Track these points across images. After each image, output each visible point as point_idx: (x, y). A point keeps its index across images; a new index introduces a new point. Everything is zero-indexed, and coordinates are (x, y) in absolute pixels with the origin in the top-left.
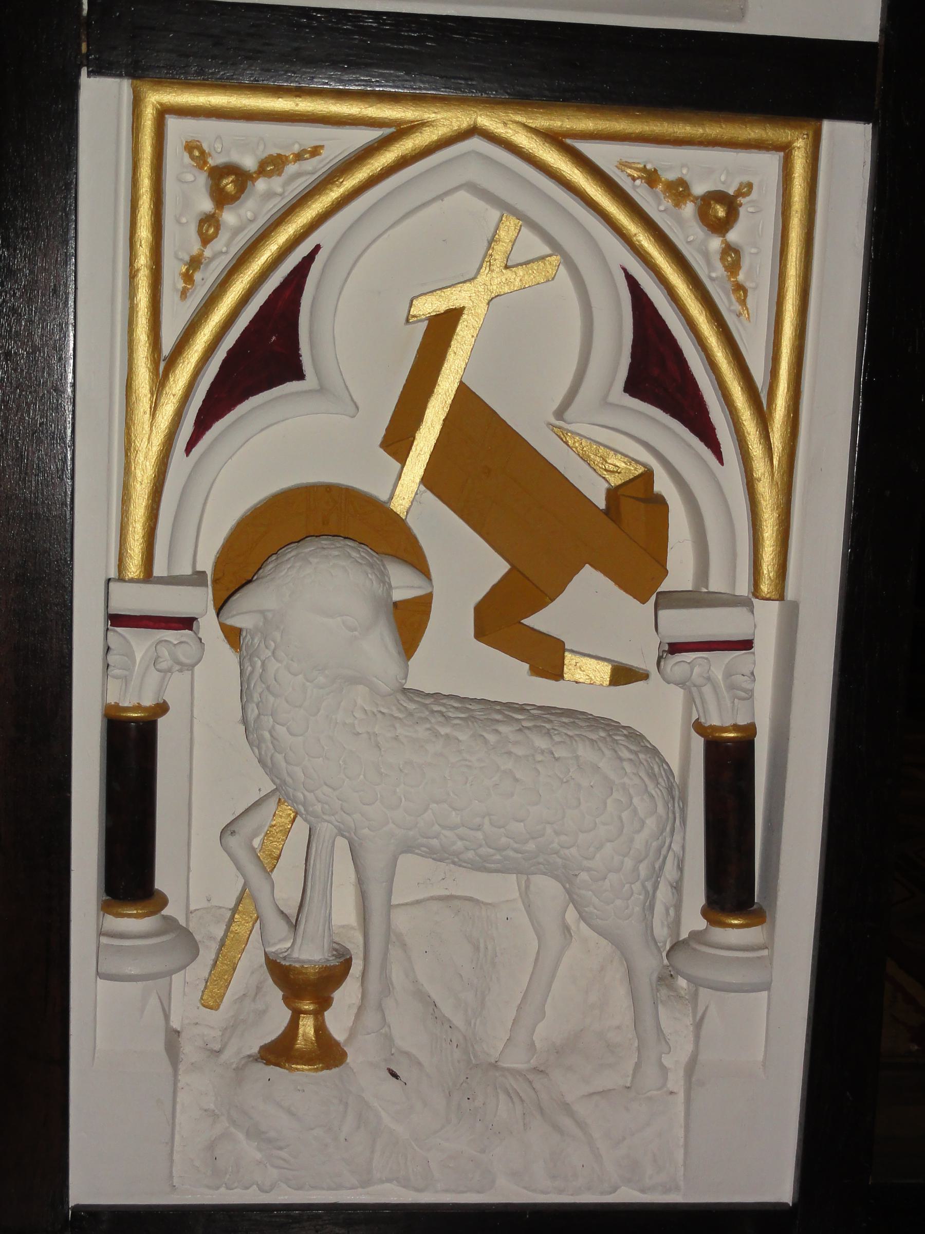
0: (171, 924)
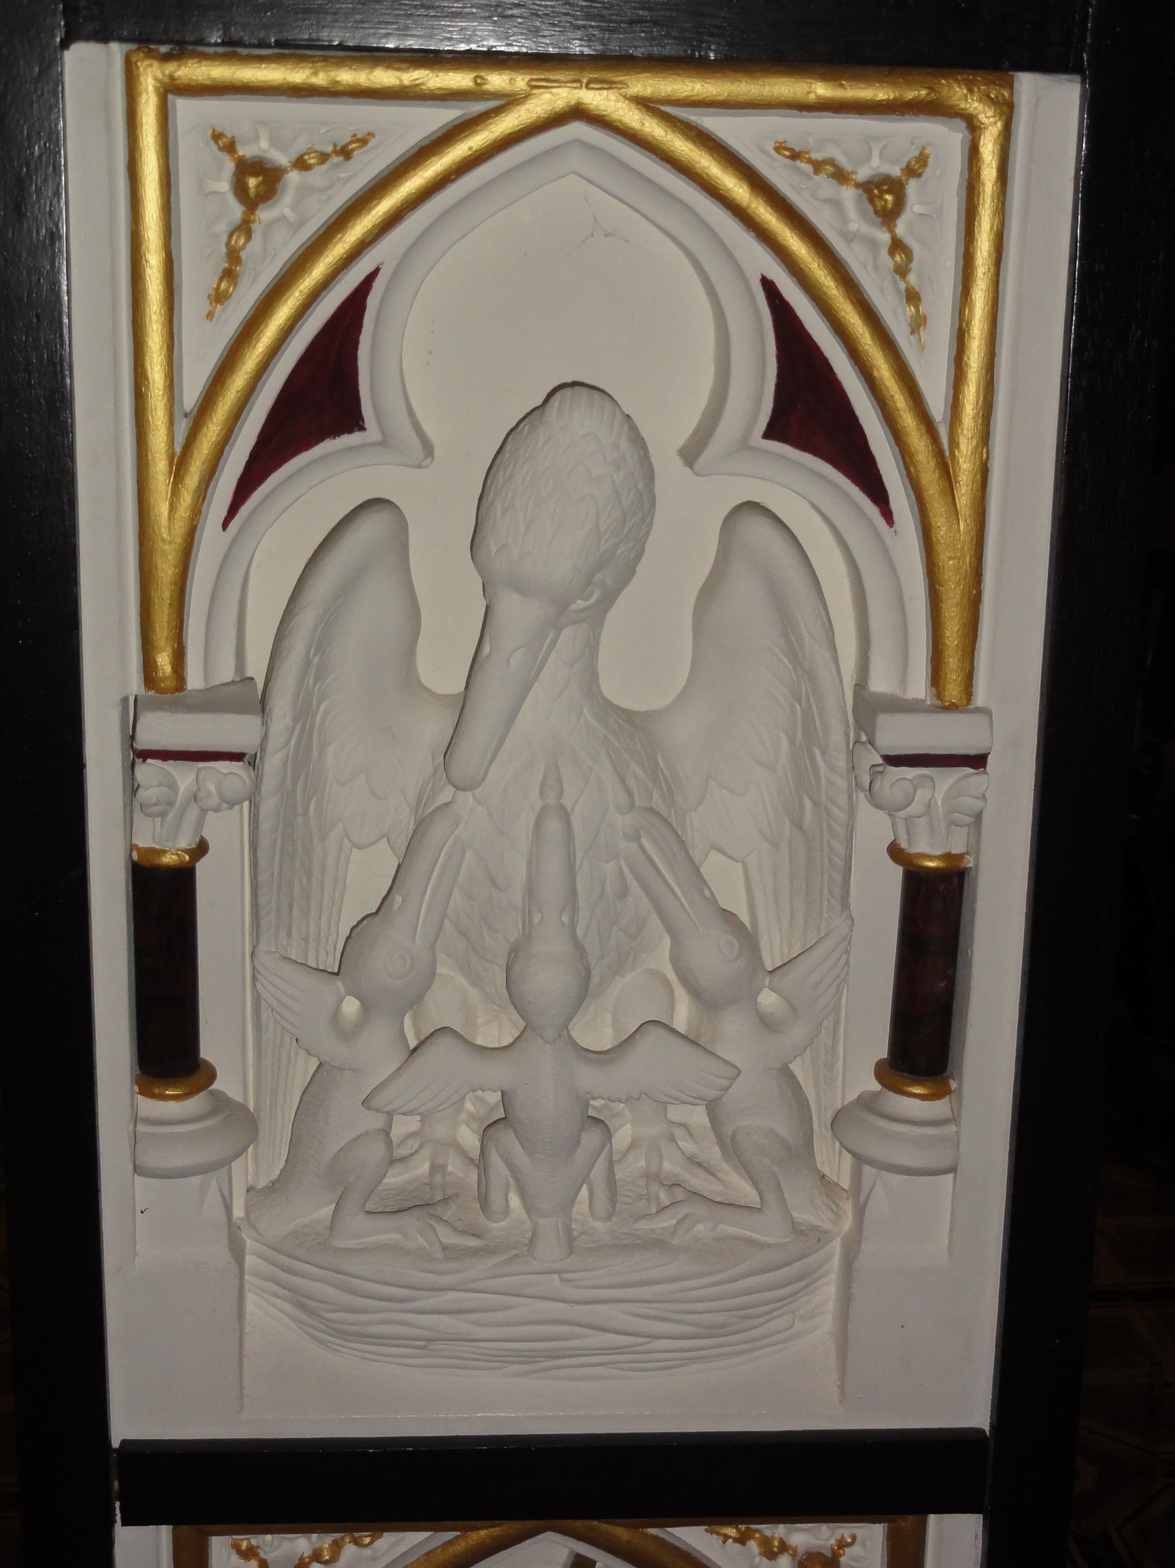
0: (222, 1104)
